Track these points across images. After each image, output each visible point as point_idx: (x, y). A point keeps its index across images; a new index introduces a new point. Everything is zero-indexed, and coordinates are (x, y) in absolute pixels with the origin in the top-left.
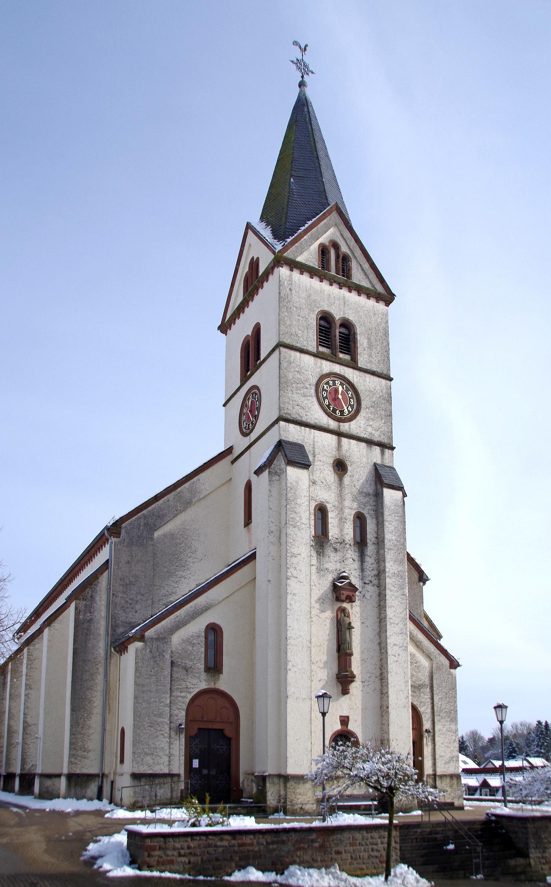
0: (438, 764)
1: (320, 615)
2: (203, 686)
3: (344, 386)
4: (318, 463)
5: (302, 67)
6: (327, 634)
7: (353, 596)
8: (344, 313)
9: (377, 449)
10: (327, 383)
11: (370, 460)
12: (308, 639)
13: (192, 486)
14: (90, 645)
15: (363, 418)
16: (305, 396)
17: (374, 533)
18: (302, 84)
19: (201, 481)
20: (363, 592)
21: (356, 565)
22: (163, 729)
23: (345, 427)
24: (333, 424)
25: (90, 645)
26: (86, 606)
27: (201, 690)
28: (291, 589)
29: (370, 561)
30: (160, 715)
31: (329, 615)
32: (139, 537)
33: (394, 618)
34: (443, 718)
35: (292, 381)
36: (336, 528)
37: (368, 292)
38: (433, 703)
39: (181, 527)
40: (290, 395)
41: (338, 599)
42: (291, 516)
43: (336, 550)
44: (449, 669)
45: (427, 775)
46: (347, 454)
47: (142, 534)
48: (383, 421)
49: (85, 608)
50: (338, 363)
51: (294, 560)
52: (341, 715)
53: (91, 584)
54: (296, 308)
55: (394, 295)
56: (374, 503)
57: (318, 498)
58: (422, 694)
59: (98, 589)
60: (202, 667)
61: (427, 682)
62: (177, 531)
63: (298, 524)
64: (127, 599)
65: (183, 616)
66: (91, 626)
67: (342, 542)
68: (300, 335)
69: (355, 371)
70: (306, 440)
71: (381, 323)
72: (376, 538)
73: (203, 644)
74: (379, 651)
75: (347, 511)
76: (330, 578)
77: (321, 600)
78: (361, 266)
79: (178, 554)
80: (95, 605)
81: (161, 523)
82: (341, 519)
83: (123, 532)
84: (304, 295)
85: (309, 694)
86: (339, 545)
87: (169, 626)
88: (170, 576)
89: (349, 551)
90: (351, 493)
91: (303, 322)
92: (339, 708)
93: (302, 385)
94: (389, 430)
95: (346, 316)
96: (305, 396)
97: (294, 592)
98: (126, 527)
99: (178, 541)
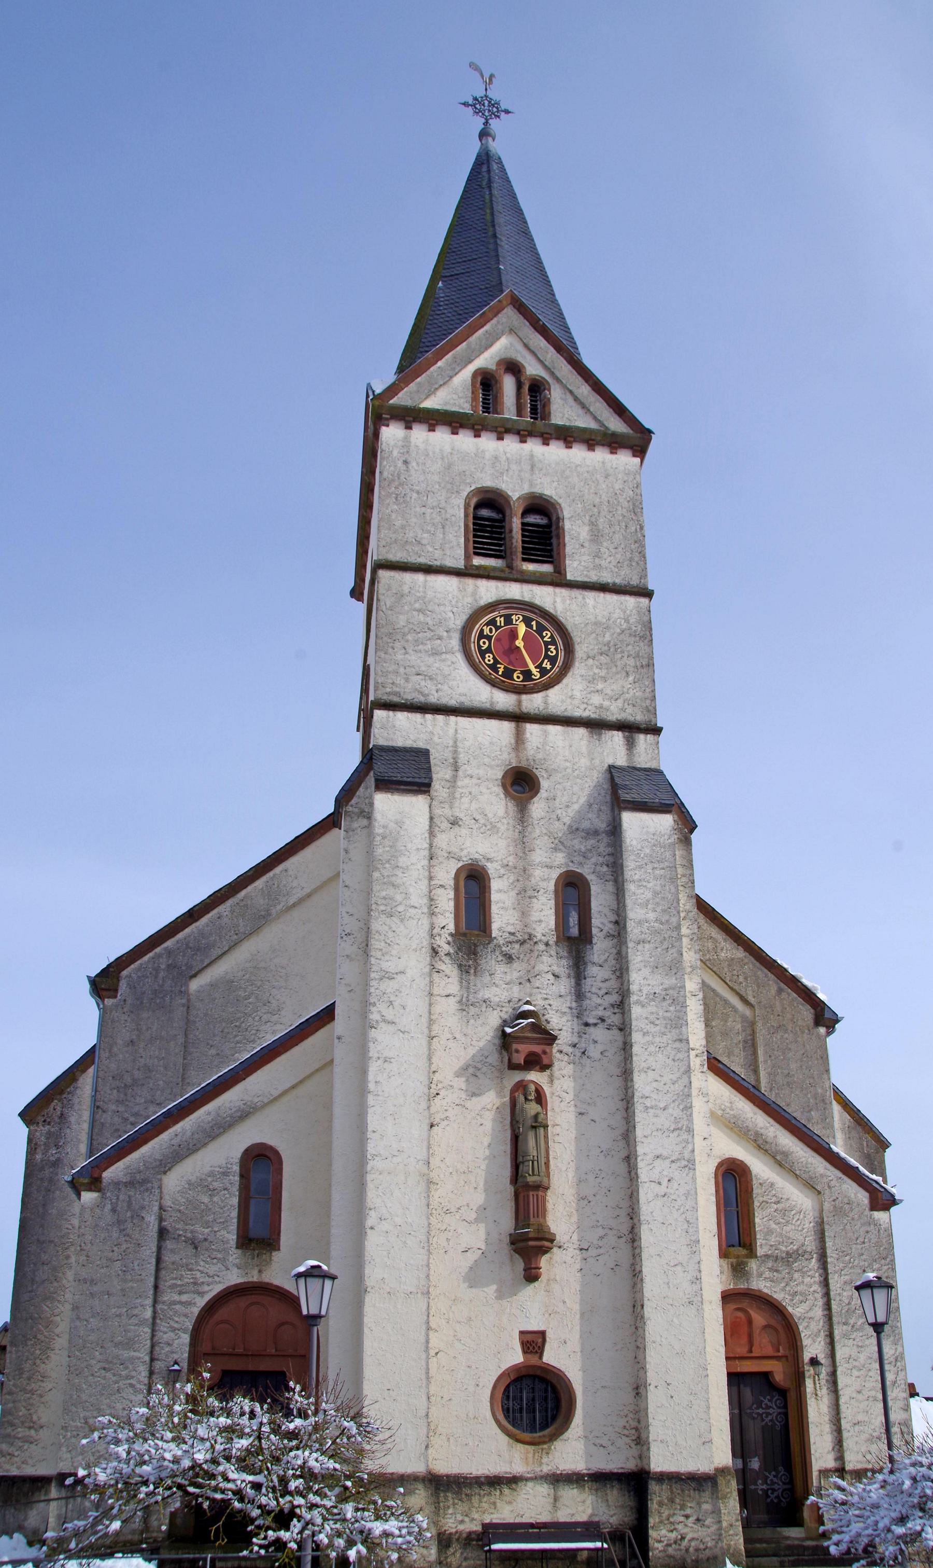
0: (848, 1444)
1: (468, 1104)
2: (234, 1278)
3: (534, 623)
4: (467, 781)
5: (487, 108)
6: (486, 1144)
7: (545, 1052)
8: (531, 485)
9: (618, 737)
10: (492, 622)
11: (597, 762)
13: (271, 883)
14: (54, 1211)
15: (580, 679)
16: (433, 654)
17: (609, 914)
18: (484, 134)
19: (290, 873)
21: (565, 986)
22: (134, 1373)
23: (533, 702)
24: (503, 700)
25: (54, 1211)
26: (49, 1135)
27: (228, 1288)
28: (379, 1048)
29: (598, 974)
30: (129, 1344)
31: (491, 1100)
32: (155, 992)
33: (654, 1096)
34: (857, 1330)
35: (406, 630)
36: (511, 912)
37: (587, 436)
38: (827, 1294)
39: (248, 965)
40: (400, 657)
41: (513, 1067)
42: (384, 894)
43: (509, 958)
44: (867, 1212)
45: (820, 1471)
46: (540, 756)
47: (162, 986)
48: (631, 679)
49: (48, 1138)
50: (516, 580)
51: (389, 986)
53: (62, 1092)
54: (418, 493)
55: (650, 432)
56: (610, 850)
58: (796, 1275)
59: (76, 1100)
60: (232, 1237)
61: (811, 1244)
62: (240, 974)
63: (400, 909)
64: (126, 1115)
65: (189, 1134)
66: (57, 1174)
67: (528, 940)
68: (424, 542)
69: (558, 590)
70: (436, 739)
71: (622, 490)
72: (617, 923)
73: (235, 1190)
74: (627, 1175)
75: (538, 873)
76: (494, 1019)
77: (471, 1071)
78: (571, 392)
79: (240, 1018)
80: (68, 1131)
81: (202, 961)
82: (522, 892)
83: (123, 986)
84: (437, 466)
86: (517, 946)
87: (158, 1157)
88: (222, 1062)
90: (550, 834)
91: (434, 516)
93: (429, 634)
94: (647, 695)
95: (538, 490)
96: (435, 653)
97: (387, 1053)
98: (129, 976)
99: (241, 993)
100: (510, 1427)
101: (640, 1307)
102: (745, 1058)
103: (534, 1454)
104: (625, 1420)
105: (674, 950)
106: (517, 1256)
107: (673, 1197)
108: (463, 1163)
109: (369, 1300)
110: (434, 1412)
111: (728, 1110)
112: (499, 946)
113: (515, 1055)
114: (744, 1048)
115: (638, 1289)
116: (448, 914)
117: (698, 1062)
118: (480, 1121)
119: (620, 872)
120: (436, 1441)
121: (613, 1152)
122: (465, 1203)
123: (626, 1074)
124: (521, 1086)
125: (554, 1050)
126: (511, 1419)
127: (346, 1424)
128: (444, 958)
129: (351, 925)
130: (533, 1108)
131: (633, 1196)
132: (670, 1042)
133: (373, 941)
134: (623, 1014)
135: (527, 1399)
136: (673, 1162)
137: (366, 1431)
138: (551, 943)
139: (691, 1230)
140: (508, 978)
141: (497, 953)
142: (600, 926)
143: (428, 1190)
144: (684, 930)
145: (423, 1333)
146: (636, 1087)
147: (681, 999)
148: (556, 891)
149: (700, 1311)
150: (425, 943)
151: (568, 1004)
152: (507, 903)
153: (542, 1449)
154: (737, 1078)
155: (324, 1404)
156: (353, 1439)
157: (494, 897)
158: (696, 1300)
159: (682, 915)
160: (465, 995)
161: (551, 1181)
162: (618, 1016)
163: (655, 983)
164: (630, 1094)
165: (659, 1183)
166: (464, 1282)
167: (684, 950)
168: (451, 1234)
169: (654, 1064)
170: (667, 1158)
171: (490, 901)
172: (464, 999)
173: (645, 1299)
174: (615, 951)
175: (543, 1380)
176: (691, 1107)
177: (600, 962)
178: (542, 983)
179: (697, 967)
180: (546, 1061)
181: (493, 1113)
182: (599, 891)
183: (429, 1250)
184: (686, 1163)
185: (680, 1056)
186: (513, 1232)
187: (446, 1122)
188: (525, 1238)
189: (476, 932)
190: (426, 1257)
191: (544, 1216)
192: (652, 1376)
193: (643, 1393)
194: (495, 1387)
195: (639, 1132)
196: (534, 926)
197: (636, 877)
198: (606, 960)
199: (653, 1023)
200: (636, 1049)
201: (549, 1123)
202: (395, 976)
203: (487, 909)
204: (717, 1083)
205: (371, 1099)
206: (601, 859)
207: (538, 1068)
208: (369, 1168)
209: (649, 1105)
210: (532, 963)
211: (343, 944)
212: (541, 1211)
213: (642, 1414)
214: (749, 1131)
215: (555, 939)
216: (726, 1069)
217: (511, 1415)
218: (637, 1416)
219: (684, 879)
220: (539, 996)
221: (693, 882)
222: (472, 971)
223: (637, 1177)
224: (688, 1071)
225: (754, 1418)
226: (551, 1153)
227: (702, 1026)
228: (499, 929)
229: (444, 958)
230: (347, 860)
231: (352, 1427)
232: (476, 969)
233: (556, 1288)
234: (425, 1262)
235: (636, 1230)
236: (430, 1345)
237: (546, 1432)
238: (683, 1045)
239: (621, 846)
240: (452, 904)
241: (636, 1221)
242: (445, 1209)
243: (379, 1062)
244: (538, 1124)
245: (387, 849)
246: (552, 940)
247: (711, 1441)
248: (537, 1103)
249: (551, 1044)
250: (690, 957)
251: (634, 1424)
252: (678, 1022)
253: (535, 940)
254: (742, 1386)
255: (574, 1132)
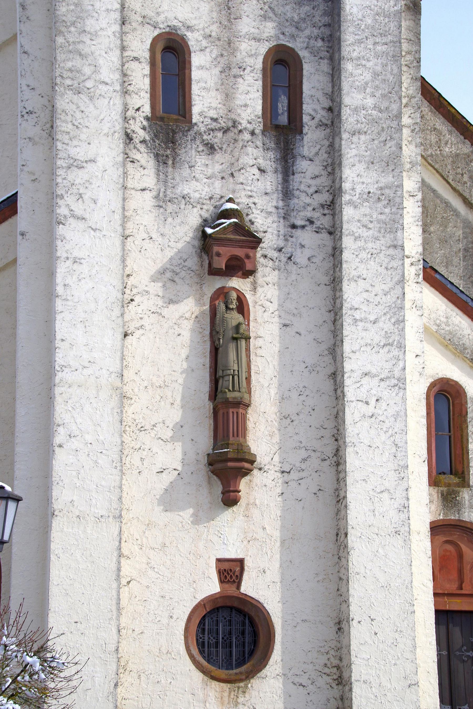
1: (165, 312)
6: (184, 356)
7: (248, 257)
12: (116, 367)
20: (288, 249)
21: (270, 182)
28: (68, 247)
29: (308, 170)
31: (189, 310)
33: (364, 307)
36: (213, 93)
41: (213, 272)
42: (69, 64)
43: (211, 148)
51: (78, 176)
52: (219, 557)
56: (326, 19)
57: (160, 19)
63: (89, 84)
67: (231, 127)
72: (330, 109)
74: (332, 393)
75: (244, 46)
76: (193, 218)
77: (168, 275)
85: (115, 505)
86: (220, 134)
89: (250, 150)
92: (215, 539)
97: (76, 253)
100: (204, 663)
101: (343, 536)
102: (465, 268)
103: (230, 693)
104: (326, 657)
105: (393, 143)
106: (215, 477)
107: (381, 418)
108: (159, 376)
109: (56, 524)
110: (123, 645)
111: (443, 326)
112: (200, 134)
113: (215, 258)
114: (465, 257)
115: (342, 516)
116: (143, 94)
117: (413, 272)
118: (177, 331)
119: (336, 48)
120: (126, 679)
121: (318, 368)
122: (161, 420)
123: (335, 283)
124: (222, 293)
125: (258, 255)
126: (206, 655)
127: (29, 659)
128: (139, 146)
129: (33, 101)
130: (234, 318)
131: (338, 417)
132: (383, 248)
133: (58, 123)
134: (333, 215)
135: (223, 632)
136: (382, 380)
137: (50, 666)
138: (257, 131)
139: (399, 454)
140: (209, 172)
141: (198, 142)
142: (313, 113)
143: (122, 406)
144: (406, 120)
145: (115, 559)
146: (345, 297)
147: (398, 200)
148: (264, 70)
149: (407, 541)
150: (118, 127)
151: (275, 204)
152: (209, 82)
153: (239, 688)
154: (454, 290)
155: (4, 638)
156: (36, 677)
157: (196, 74)
158: (404, 530)
159: (404, 101)
160: (162, 190)
161: (253, 398)
162: (328, 218)
163: (369, 180)
164: (338, 305)
165: (367, 403)
166: (159, 505)
167: (404, 143)
168: (145, 453)
169: (365, 272)
170: (375, 376)
171: (190, 79)
172: (161, 195)
173: (350, 527)
174: (327, 143)
175: (240, 611)
176: (403, 321)
177: (311, 156)
178: (247, 179)
179: (417, 163)
180: (249, 267)
181: (192, 322)
182: (313, 70)
183: (121, 471)
184: (396, 382)
185: (394, 264)
186: (211, 451)
187: (141, 331)
188: (224, 459)
189: (175, 117)
190: (118, 478)
191: (244, 436)
192: (356, 610)
193: (346, 629)
194: (186, 638)
195: (347, 347)
196: (239, 111)
197: (355, 55)
198: (317, 154)
199: (365, 226)
200: (346, 255)
201: (251, 335)
202: (85, 164)
203: (187, 90)
204: (432, 295)
205: (59, 304)
206: (316, 31)
207: (240, 273)
208: (57, 380)
209: (358, 317)
210: (236, 154)
211: (24, 124)
212: (241, 430)
213: (344, 651)
214: (465, 349)
215: (261, 127)
216: (443, 281)
217: (206, 649)
218: (338, 654)
219: (409, 58)
220: (243, 193)
221: (419, 61)
222: (170, 162)
223: (344, 396)
224: (402, 281)
225: (464, 661)
226: (252, 367)
227: (419, 230)
228: (201, 114)
229: (139, 146)
230: (25, 19)
231: (35, 662)
232: (174, 159)
233: (255, 513)
234: (117, 484)
235: (341, 453)
236: (122, 573)
237: (243, 669)
238: (397, 252)
239: (339, 15)
240: (147, 81)
241: (341, 442)
242: (139, 426)
243: (69, 263)
244: (240, 336)
245: (72, 7)
246: (259, 129)
247: (417, 684)
248: (239, 312)
249: (255, 248)
250: (410, 152)
251: (335, 662)
252: (393, 226)
253: (240, 128)
254: (451, 625)
255: (278, 345)
